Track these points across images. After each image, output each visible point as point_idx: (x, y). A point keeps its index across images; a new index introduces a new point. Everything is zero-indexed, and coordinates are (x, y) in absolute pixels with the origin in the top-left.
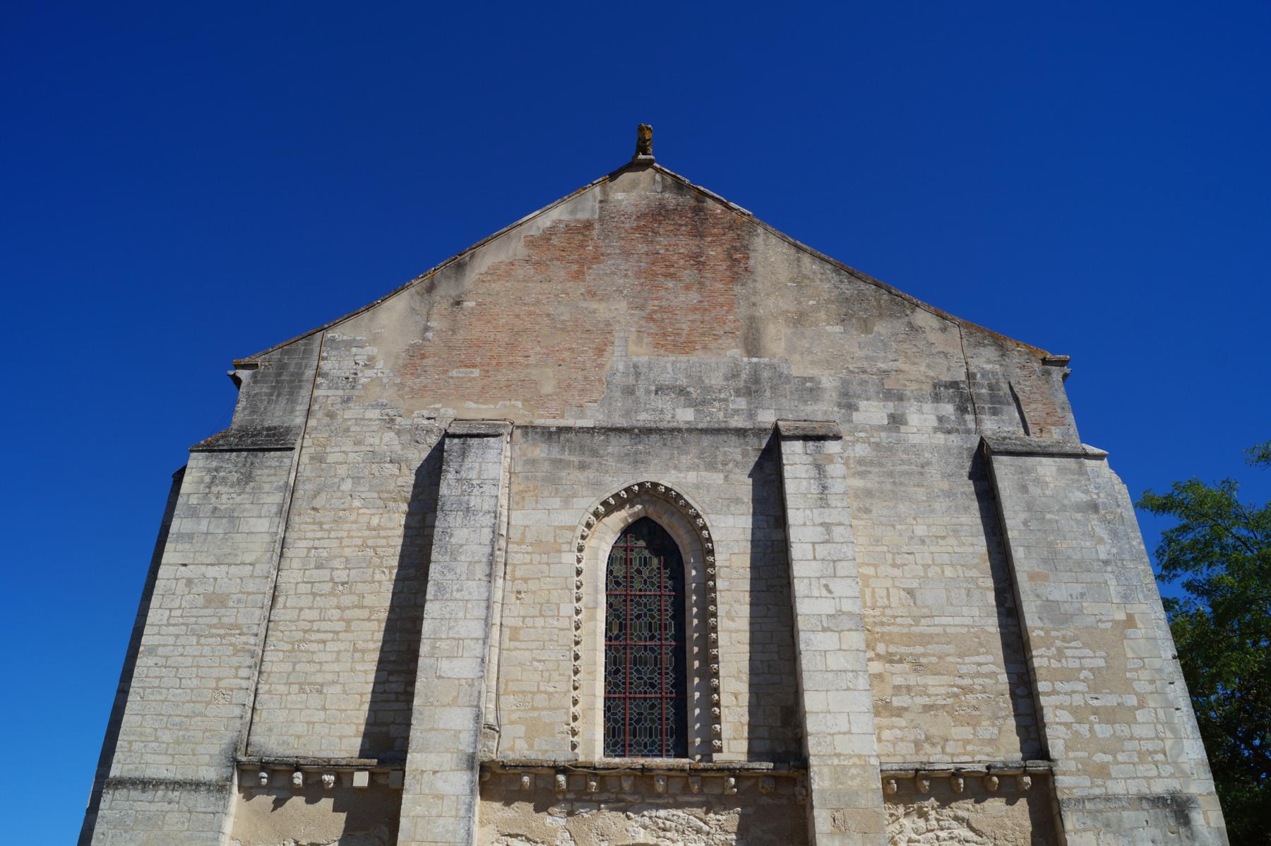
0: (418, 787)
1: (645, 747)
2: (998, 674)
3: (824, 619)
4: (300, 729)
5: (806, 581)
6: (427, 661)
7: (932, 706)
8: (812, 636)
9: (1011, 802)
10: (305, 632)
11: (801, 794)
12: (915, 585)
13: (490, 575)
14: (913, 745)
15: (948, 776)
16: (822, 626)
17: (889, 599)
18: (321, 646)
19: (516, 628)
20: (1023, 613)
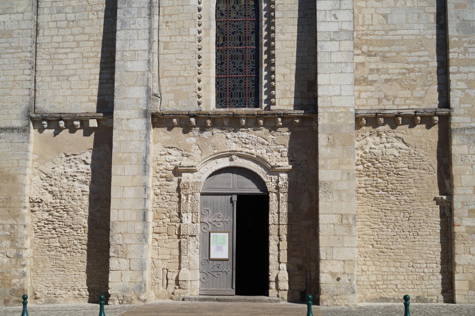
0: (120, 127)
1: (237, 102)
2: (429, 62)
3: (332, 34)
4: (60, 99)
5: (323, 12)
6: (120, 63)
7: (390, 80)
8: (324, 44)
9: (428, 127)
10: (56, 48)
11: (315, 126)
12: (388, 12)
13: (150, 15)
14: (377, 100)
15: (394, 116)
16: (331, 38)
17: (372, 21)
18: (65, 56)
19: (167, 42)
20: (448, 28)
